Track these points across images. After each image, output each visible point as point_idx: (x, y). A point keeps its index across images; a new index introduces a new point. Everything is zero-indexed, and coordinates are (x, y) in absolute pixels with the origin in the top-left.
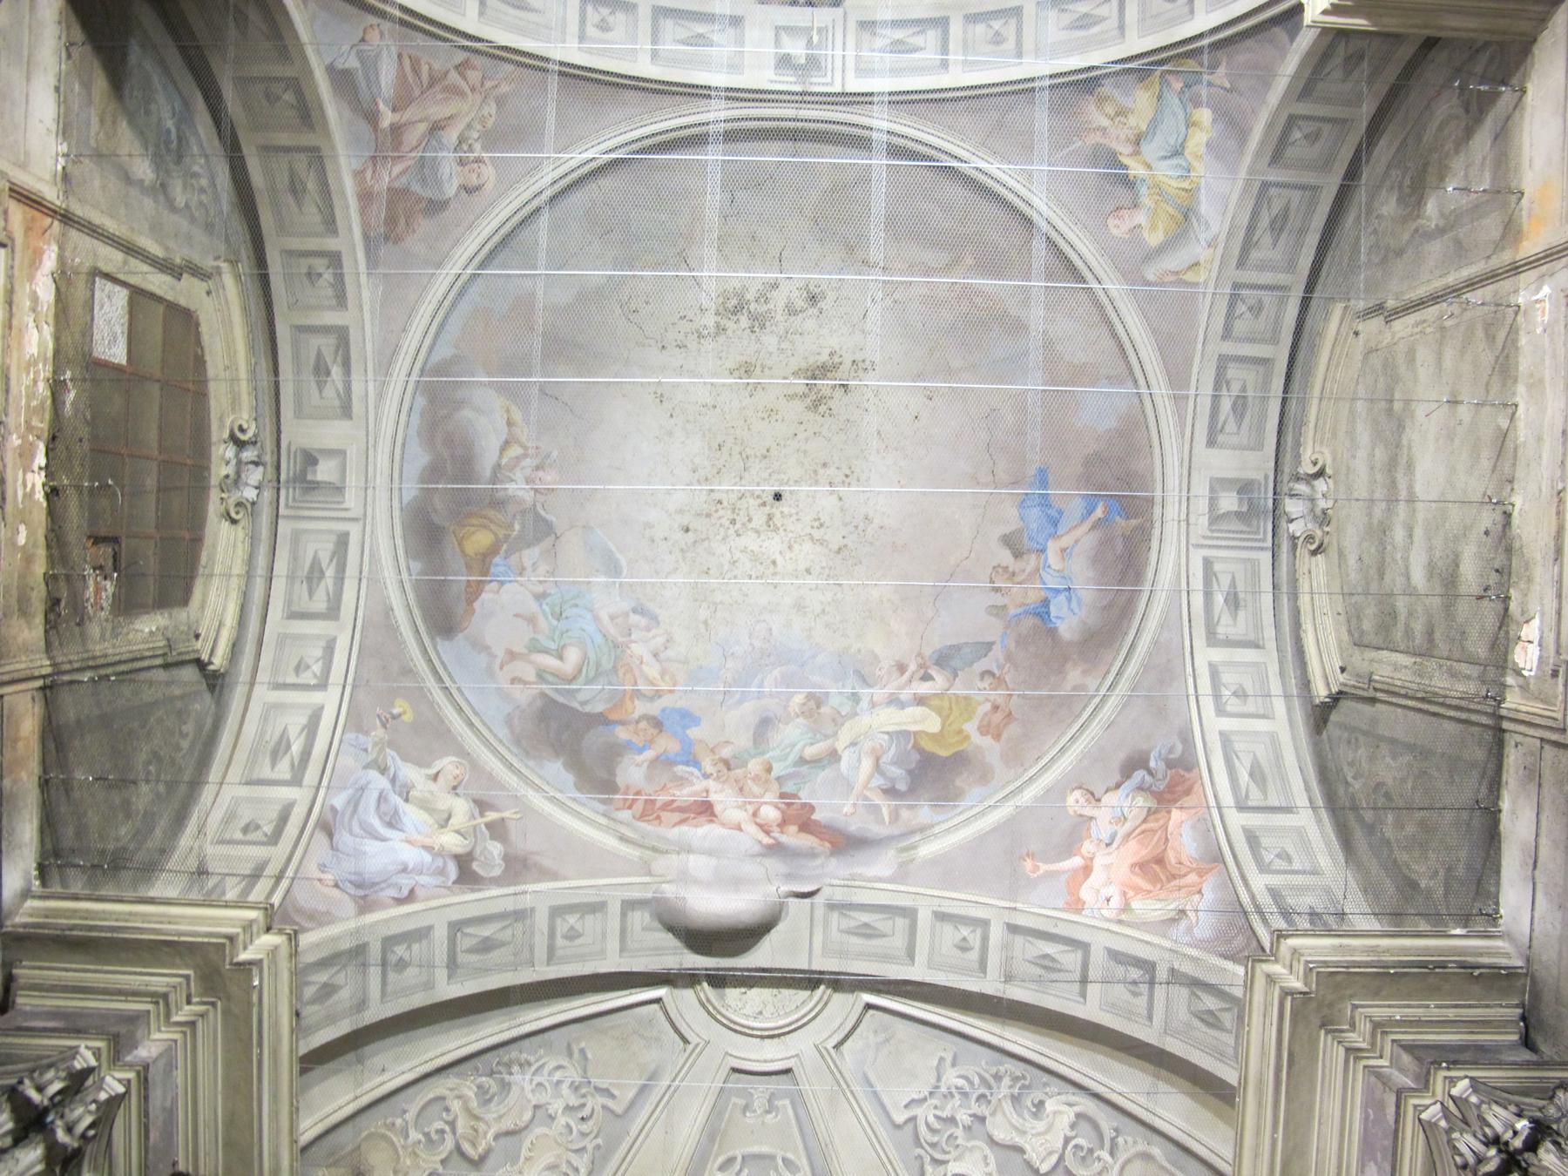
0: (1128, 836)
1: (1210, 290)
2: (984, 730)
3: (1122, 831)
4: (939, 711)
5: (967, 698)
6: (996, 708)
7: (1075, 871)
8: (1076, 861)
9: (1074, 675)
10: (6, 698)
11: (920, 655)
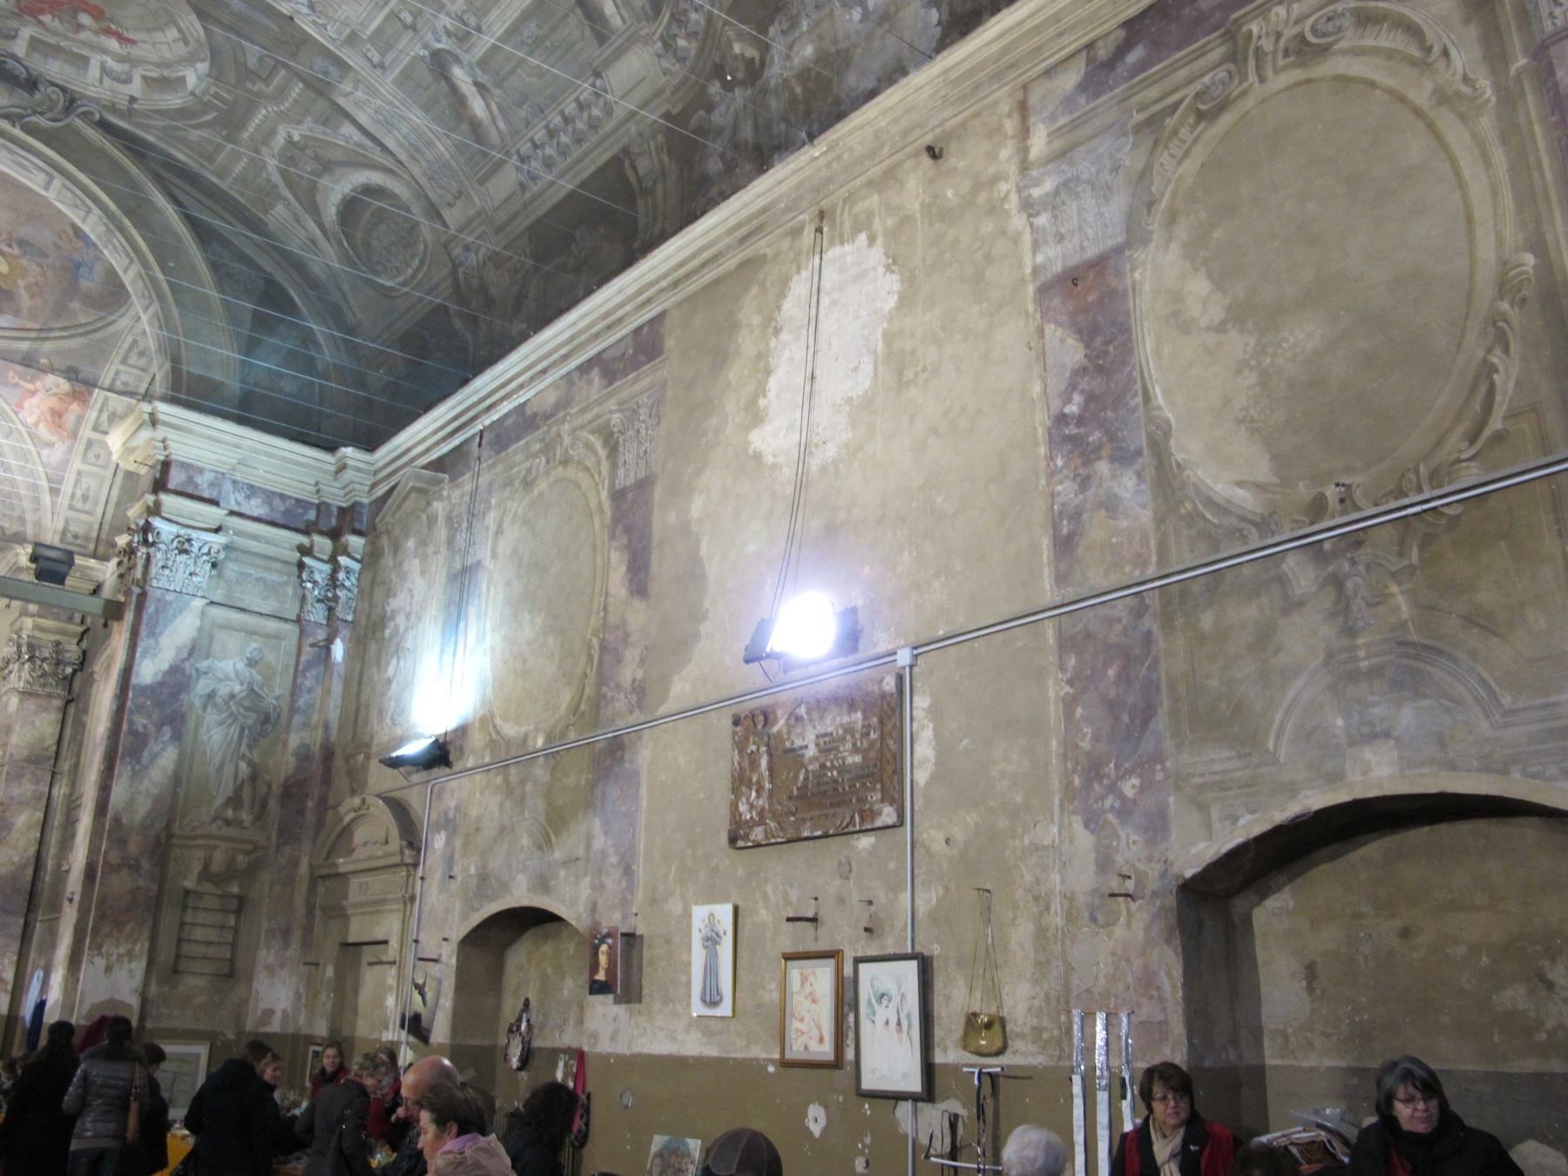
0: (55, 394)
1: (620, 41)
2: (28, 288)
3: (55, 390)
4: (10, 264)
5: (26, 270)
6: (37, 284)
7: (29, 391)
8: (30, 386)
9: (763, 875)
10: (354, 882)
11: (10, 233)
